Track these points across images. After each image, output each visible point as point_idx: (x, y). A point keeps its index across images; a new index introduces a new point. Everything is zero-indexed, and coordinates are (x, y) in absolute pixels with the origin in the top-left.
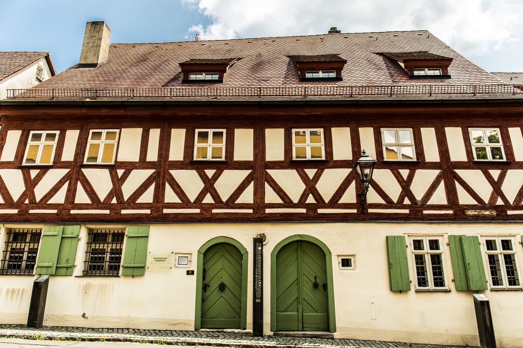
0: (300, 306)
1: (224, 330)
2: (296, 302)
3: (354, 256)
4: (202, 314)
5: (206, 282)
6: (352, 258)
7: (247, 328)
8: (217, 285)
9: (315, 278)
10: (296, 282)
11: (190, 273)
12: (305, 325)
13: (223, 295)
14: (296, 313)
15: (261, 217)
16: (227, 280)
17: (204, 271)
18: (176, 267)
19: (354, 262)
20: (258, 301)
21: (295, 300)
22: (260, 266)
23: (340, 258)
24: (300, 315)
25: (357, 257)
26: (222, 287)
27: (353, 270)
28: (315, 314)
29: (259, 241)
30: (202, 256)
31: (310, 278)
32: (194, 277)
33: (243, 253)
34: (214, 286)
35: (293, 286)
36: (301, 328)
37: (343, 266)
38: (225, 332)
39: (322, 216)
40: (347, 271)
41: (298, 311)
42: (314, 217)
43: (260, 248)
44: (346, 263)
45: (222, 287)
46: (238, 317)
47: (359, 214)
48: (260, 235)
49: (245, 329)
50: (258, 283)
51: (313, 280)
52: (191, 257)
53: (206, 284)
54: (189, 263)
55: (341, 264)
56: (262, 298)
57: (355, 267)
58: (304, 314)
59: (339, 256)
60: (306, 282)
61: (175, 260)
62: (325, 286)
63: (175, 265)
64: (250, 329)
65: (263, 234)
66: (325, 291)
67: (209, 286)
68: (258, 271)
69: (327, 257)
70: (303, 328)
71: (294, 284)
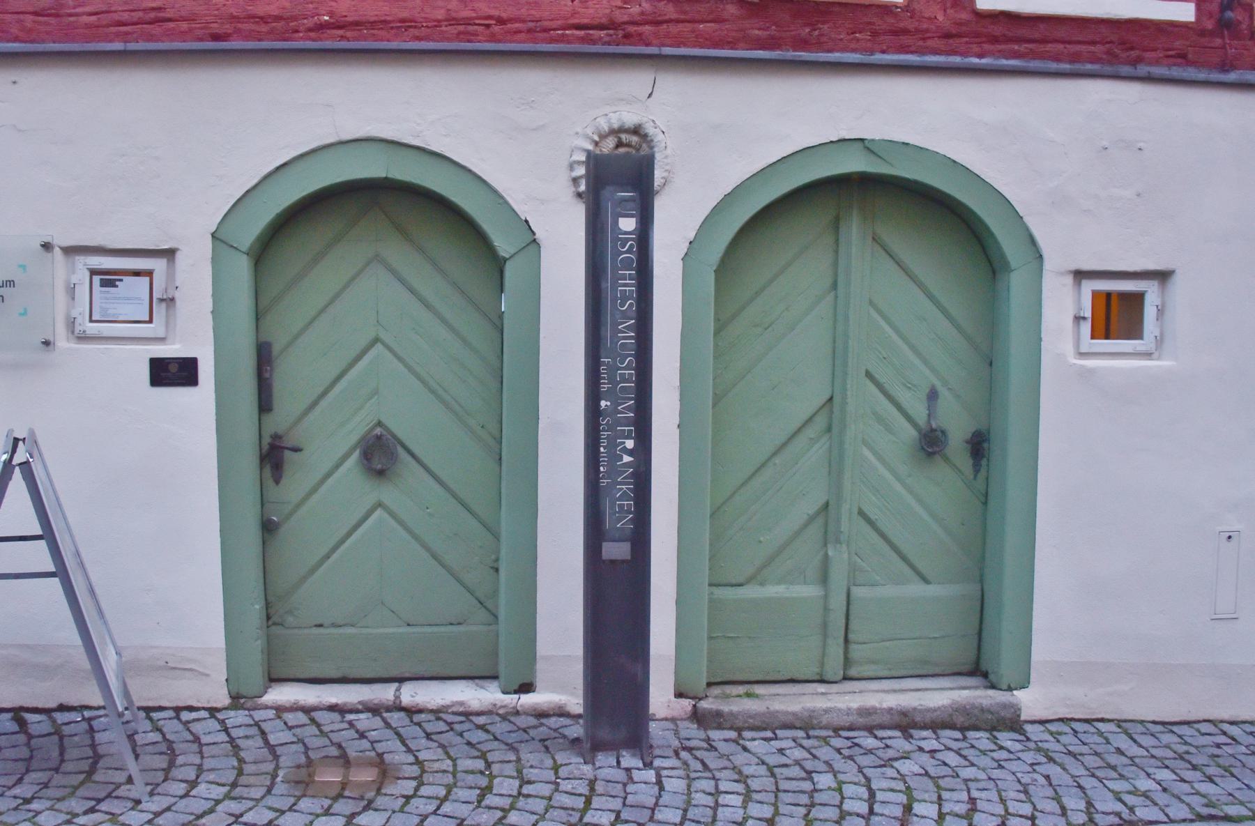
0: (839, 557)
1: (412, 694)
2: (815, 531)
3: (1163, 276)
4: (268, 605)
5: (279, 420)
6: (1152, 292)
7: (539, 684)
8: (357, 428)
9: (933, 395)
10: (821, 422)
11: (173, 373)
12: (856, 651)
13: (388, 493)
14: (810, 591)
15: (621, 17)
16: (410, 416)
17: (264, 357)
18: (83, 338)
19: (1161, 311)
20: (616, 550)
21: (811, 519)
22: (627, 337)
23: (1089, 287)
24: (837, 602)
25: (1177, 282)
26: (379, 454)
27: (1148, 355)
28: (916, 589)
29: (620, 177)
30: (243, 266)
31: (904, 397)
32: (198, 402)
33: (503, 246)
34: (328, 442)
35: (802, 440)
36: (834, 667)
37: (1133, 329)
38: (411, 711)
39: (997, 30)
40: (1117, 360)
41: (824, 578)
42: (947, 36)
43: (628, 224)
44: (1117, 315)
45: (379, 454)
46: (482, 615)
47: (1202, 33)
48: (614, 132)
49: (527, 688)
50: (612, 444)
51: (919, 411)
52: (171, 274)
53: (276, 437)
54: (160, 311)
55: (1086, 328)
56: (640, 538)
57: (1160, 341)
58: (857, 592)
59: (1080, 275)
60: (880, 419)
61: (71, 291)
62: (979, 446)
63: (71, 323)
64: (561, 686)
65: (636, 130)
66: (977, 468)
67: (296, 450)
68: (613, 369)
69: (1017, 281)
70: (847, 662)
71: (810, 432)
